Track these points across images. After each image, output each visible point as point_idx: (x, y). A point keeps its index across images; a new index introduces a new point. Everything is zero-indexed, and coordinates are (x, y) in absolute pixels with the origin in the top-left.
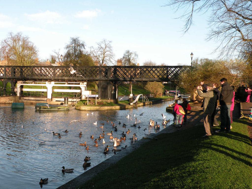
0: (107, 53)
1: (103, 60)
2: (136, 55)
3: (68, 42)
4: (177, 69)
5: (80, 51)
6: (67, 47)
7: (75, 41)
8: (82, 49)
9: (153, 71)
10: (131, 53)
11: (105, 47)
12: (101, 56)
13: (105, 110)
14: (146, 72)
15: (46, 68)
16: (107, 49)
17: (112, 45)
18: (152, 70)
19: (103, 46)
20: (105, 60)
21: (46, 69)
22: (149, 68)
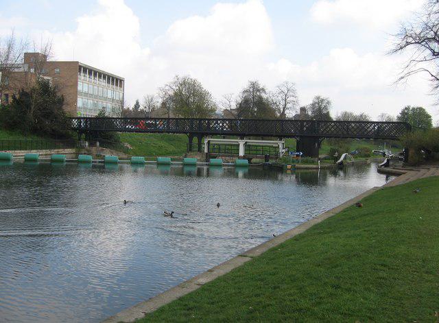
2: (328, 103)
3: (246, 86)
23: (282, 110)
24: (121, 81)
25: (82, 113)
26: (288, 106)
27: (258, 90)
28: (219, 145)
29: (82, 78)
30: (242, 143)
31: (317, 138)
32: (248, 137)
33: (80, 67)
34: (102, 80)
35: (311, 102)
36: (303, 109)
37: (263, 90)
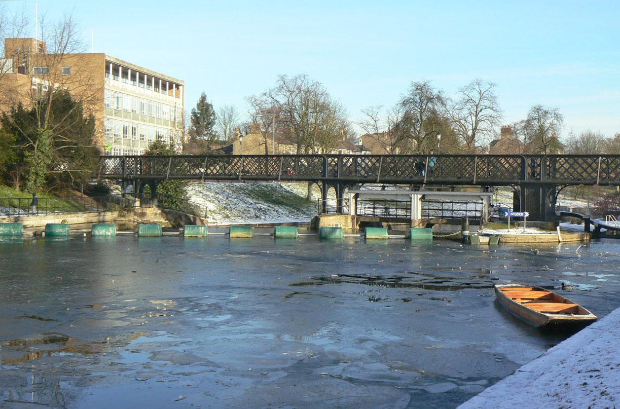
0: (483, 113)
1: (474, 130)
2: (557, 117)
3: (406, 91)
4: (235, 160)
5: (434, 112)
6: (404, 104)
7: (421, 89)
8: (439, 108)
9: (587, 163)
10: (546, 112)
11: (479, 96)
12: (469, 119)
13: (211, 304)
14: (587, 170)
15: (294, 159)
16: (486, 103)
17: (496, 91)
18: (576, 161)
19: (476, 96)
20: (478, 130)
21: (499, 162)
22: (359, 158)
23: (470, 133)
24: (178, 86)
25: (121, 149)
26: (481, 125)
27: (430, 100)
28: (411, 209)
29: (480, 142)
30: (416, 198)
31: (555, 185)
32: (439, 185)
33: (108, 64)
34: (129, 81)
35: (525, 118)
36: (506, 130)
37: (439, 98)
